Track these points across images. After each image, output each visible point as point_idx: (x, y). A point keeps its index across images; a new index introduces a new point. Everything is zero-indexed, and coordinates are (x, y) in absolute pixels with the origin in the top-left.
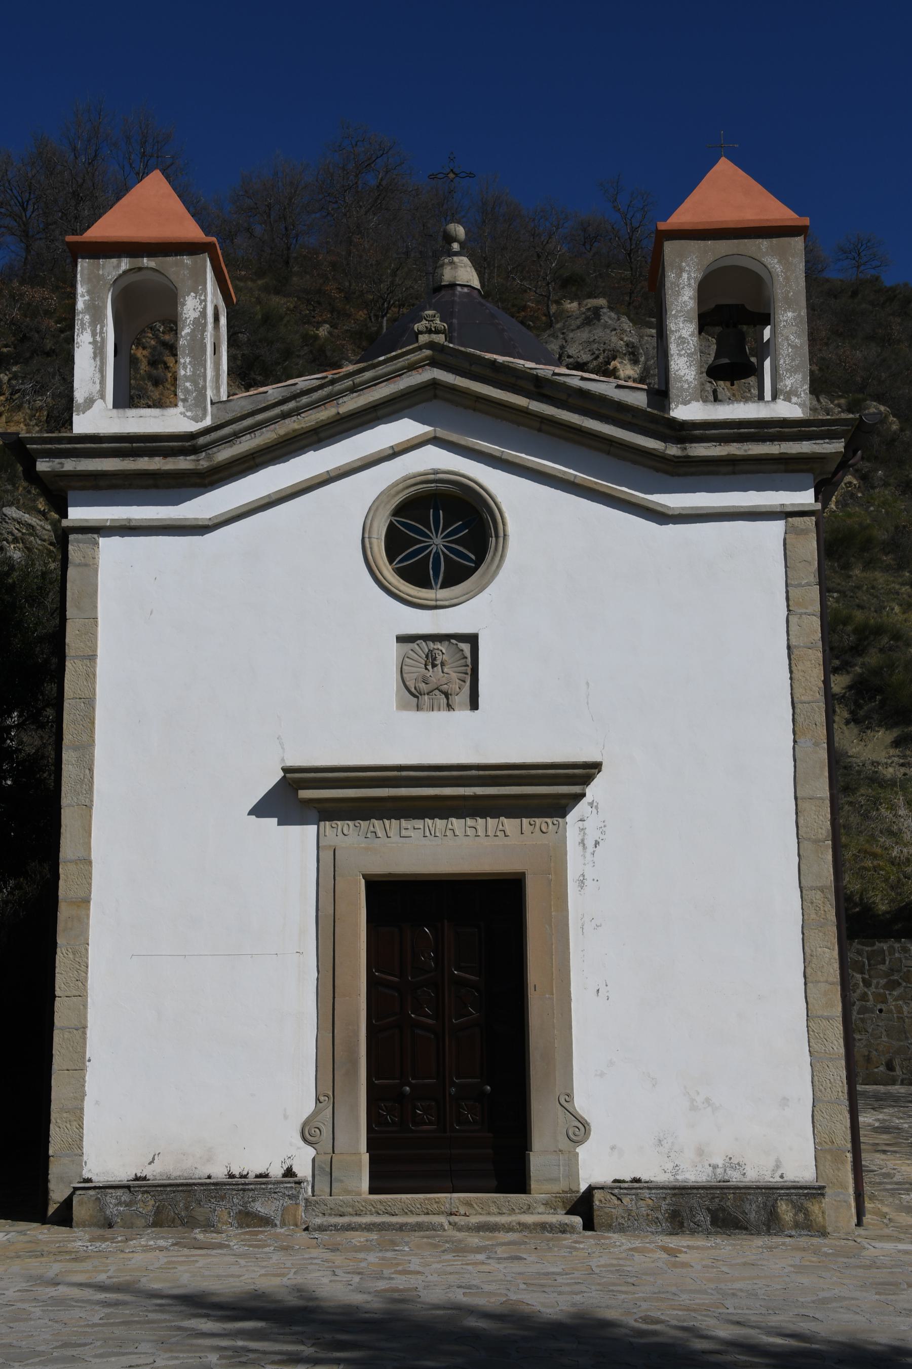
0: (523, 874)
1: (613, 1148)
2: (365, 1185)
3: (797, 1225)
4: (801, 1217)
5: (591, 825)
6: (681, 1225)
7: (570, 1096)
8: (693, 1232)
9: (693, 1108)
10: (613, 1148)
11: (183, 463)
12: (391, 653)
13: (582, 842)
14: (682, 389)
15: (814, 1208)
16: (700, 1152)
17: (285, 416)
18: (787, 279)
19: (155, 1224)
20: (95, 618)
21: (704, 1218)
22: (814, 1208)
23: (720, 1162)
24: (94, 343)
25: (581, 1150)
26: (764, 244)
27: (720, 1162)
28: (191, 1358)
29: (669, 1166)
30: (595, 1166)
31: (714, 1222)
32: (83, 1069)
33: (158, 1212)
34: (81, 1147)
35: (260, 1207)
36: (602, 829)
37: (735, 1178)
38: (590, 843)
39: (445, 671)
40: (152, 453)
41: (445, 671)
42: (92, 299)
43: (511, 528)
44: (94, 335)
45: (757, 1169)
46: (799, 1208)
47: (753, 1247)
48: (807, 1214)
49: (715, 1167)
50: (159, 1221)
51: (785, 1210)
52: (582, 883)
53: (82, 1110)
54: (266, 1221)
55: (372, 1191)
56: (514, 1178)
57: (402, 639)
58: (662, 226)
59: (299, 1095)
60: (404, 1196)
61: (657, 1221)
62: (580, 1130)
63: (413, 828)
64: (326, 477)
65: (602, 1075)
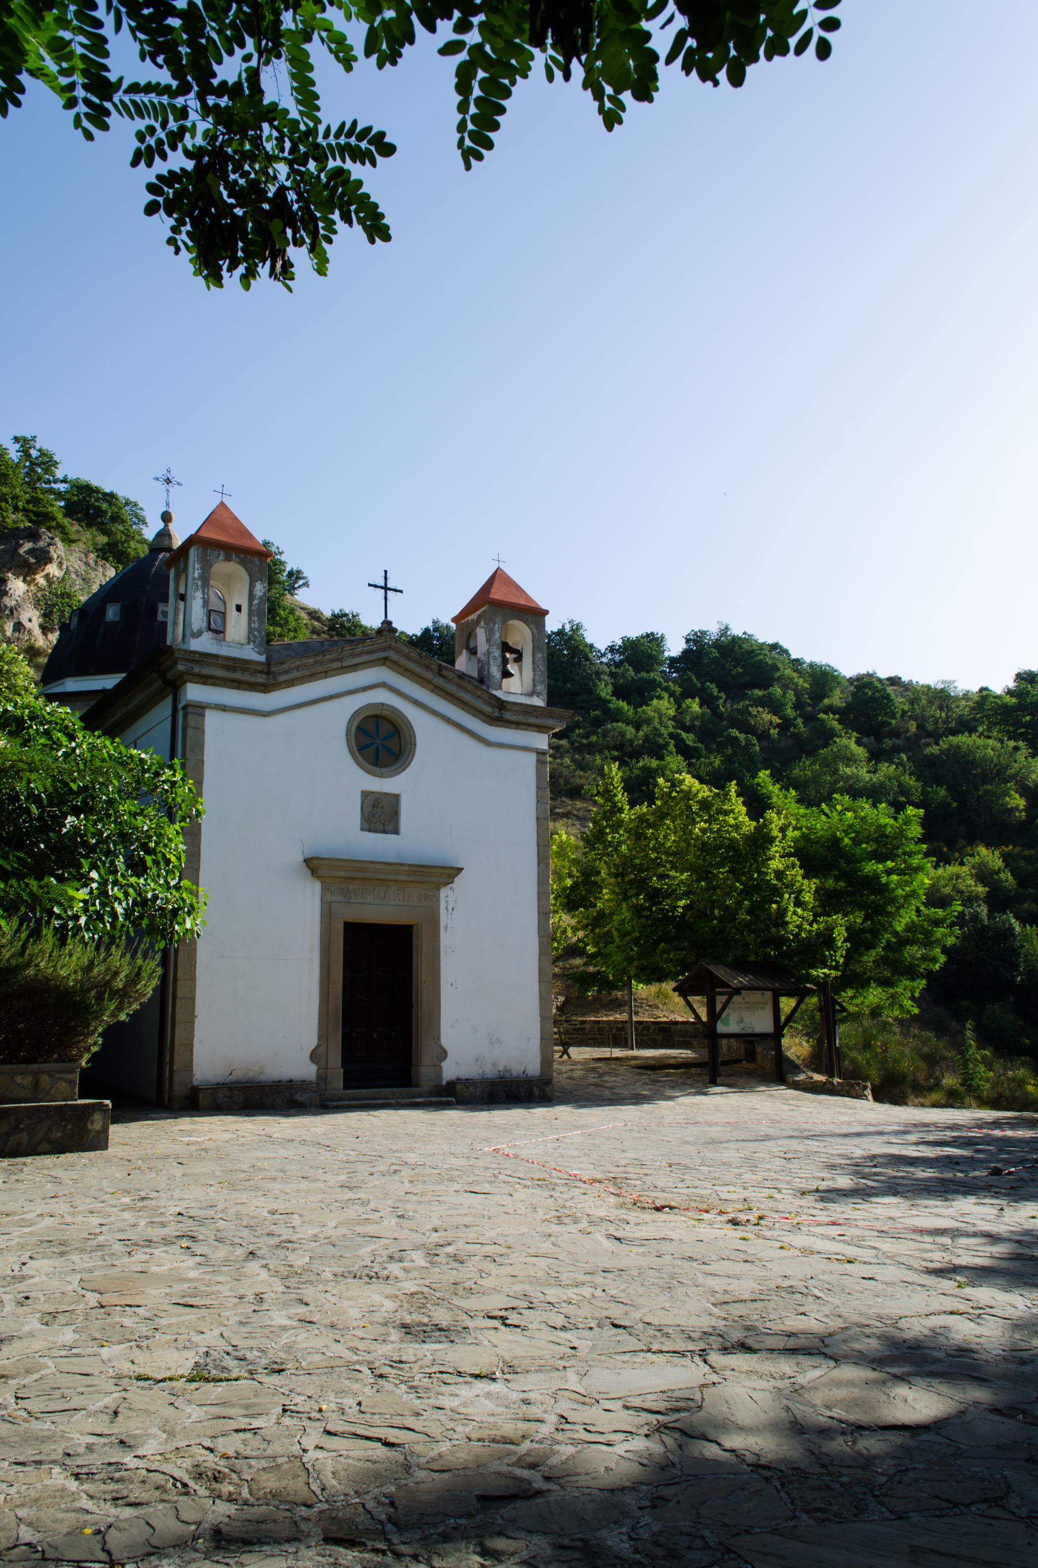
2: (340, 1084)
5: (451, 899)
7: (439, 1037)
9: (492, 1043)
15: (548, 1089)
20: (203, 761)
24: (203, 598)
25: (443, 1064)
28: (1013, 1124)
30: (450, 1070)
32: (193, 1022)
34: (192, 1066)
36: (456, 902)
38: (450, 909)
39: (380, 814)
41: (380, 814)
42: (203, 573)
44: (203, 594)
52: (446, 929)
53: (192, 1045)
55: (345, 1088)
59: (308, 1035)
60: (401, 1089)
62: (443, 1054)
65: (453, 1027)
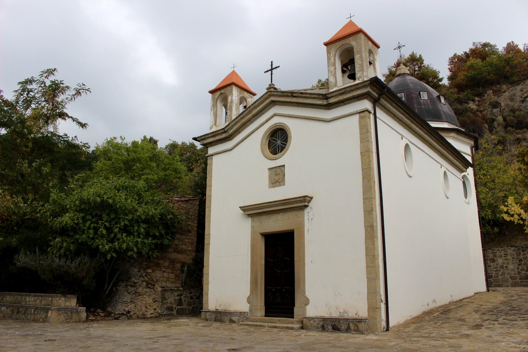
0: (293, 230)
1: (315, 306)
3: (355, 330)
4: (356, 328)
6: (324, 329)
8: (327, 331)
10: (315, 306)
11: (224, 136)
12: (267, 173)
13: (309, 219)
14: (332, 85)
16: (337, 308)
17: (242, 119)
18: (357, 46)
19: (215, 321)
21: (330, 327)
22: (360, 325)
23: (342, 311)
26: (351, 39)
27: (342, 311)
29: (329, 312)
31: (333, 329)
32: (208, 284)
33: (216, 318)
35: (233, 318)
37: (346, 316)
39: (277, 177)
40: (218, 135)
41: (277, 177)
43: (292, 134)
45: (351, 314)
46: (356, 325)
47: (343, 336)
48: (358, 327)
49: (341, 313)
50: (216, 320)
51: (352, 326)
52: (308, 231)
54: (234, 322)
56: (291, 314)
57: (269, 169)
58: (207, 155)
59: (245, 289)
61: (318, 328)
63: (274, 217)
64: (284, 103)
